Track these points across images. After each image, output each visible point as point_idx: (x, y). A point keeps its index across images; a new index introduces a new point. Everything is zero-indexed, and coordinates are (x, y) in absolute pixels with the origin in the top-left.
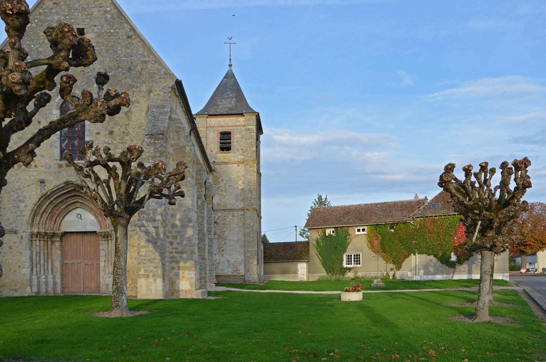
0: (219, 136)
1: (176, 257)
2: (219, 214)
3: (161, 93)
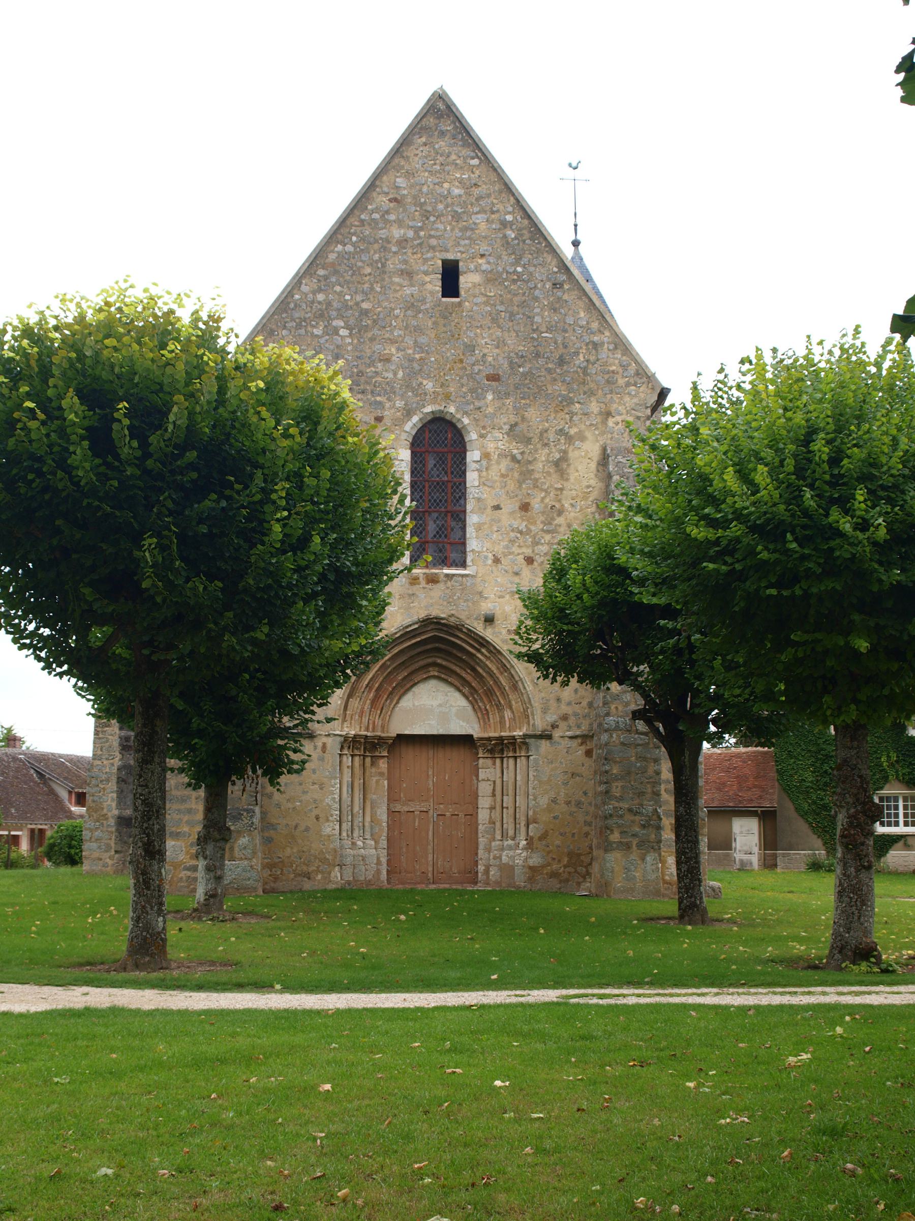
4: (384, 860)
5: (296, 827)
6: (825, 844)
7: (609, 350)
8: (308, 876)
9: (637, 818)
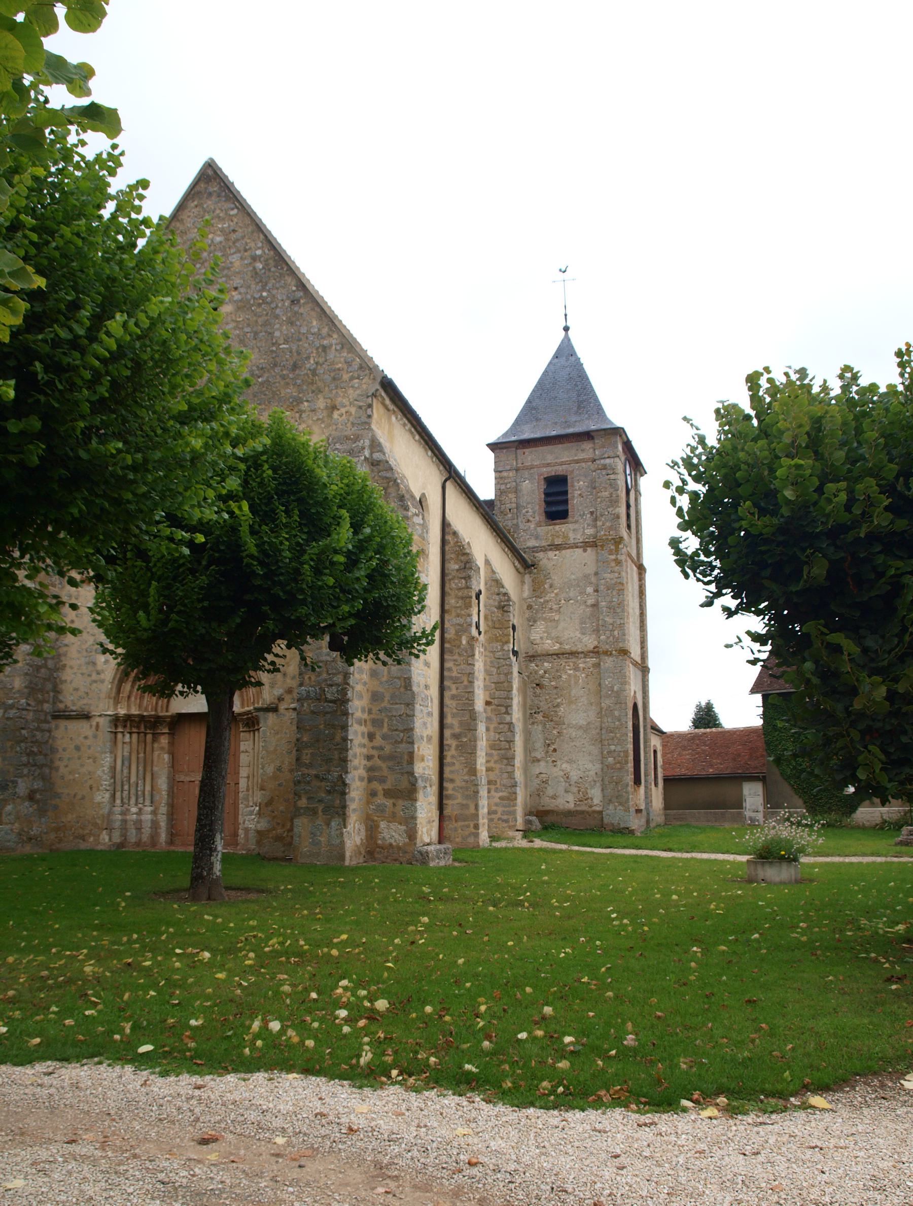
0: (543, 486)
1: (380, 769)
2: (546, 664)
3: (353, 410)
4: (163, 824)
5: (75, 796)
6: (805, 802)
7: (336, 350)
8: (83, 838)
9: (323, 784)
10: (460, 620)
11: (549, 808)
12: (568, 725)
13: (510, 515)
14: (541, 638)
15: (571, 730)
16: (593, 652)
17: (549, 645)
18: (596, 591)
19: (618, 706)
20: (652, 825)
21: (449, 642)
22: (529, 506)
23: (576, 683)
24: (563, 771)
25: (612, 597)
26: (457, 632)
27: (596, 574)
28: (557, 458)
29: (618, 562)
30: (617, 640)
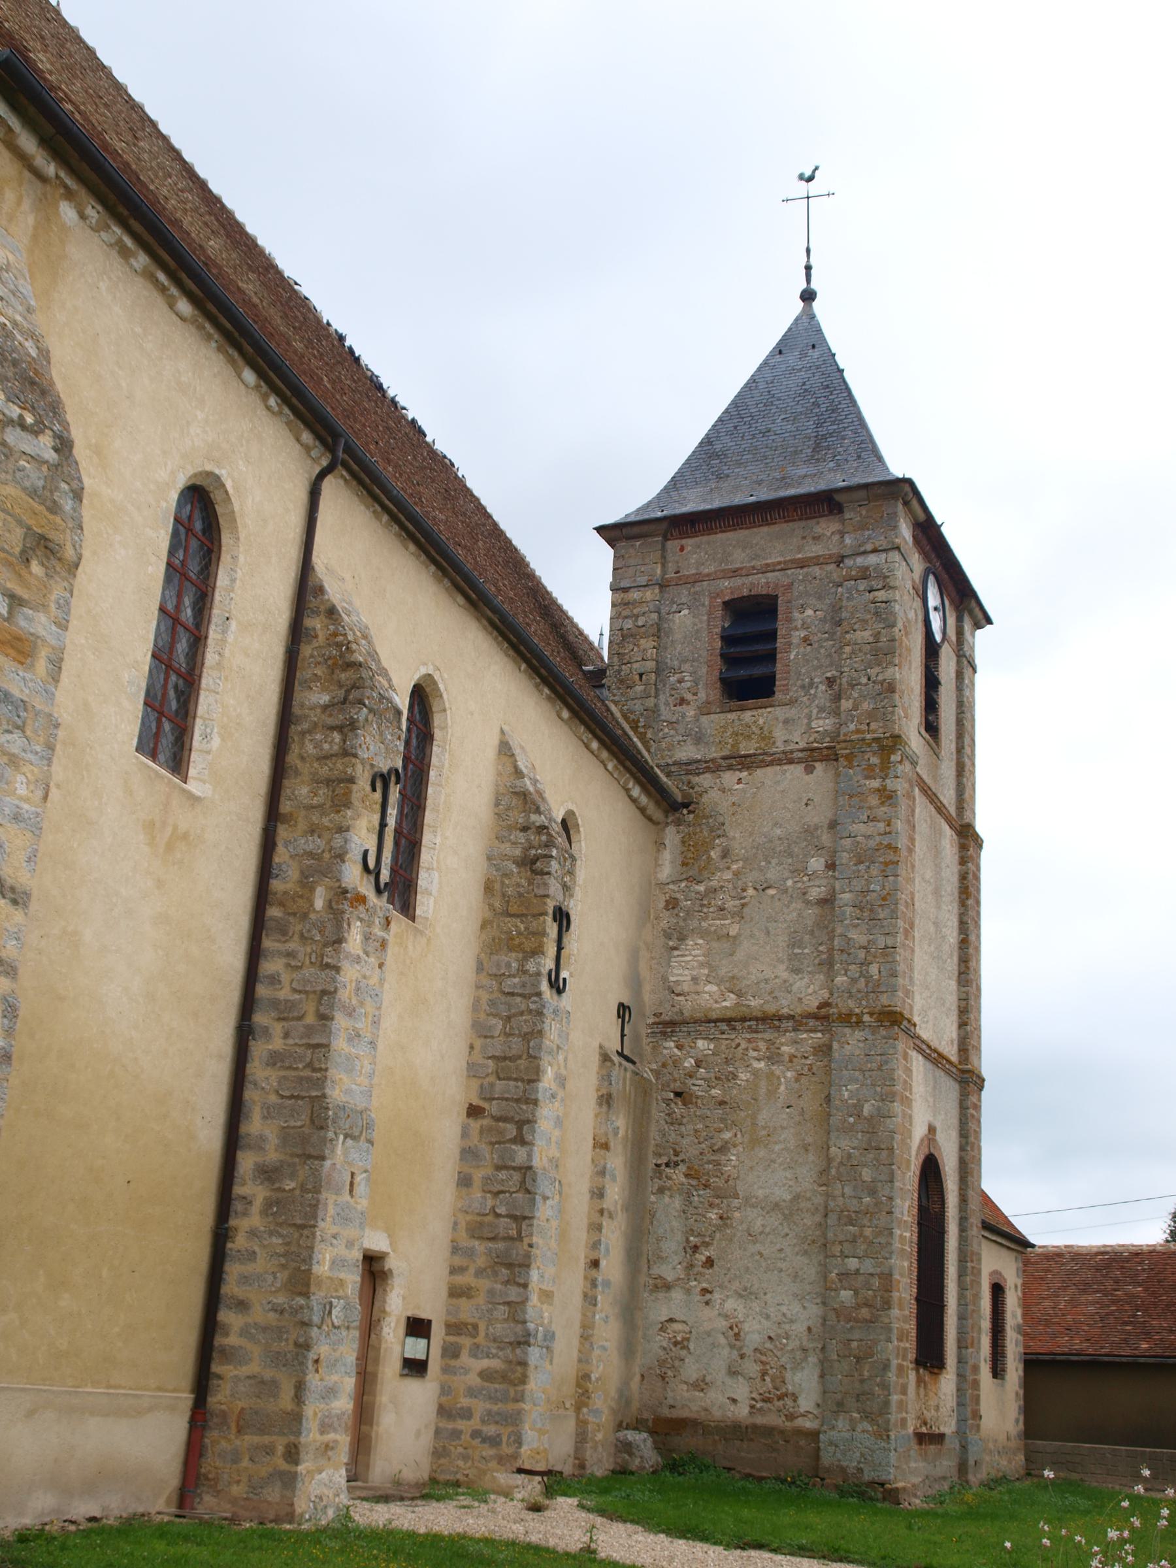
0: (720, 622)
2: (701, 1044)
10: (315, 843)
11: (685, 1414)
12: (747, 1199)
13: (639, 688)
14: (695, 979)
15: (751, 1213)
16: (815, 1017)
17: (712, 998)
18: (831, 866)
19: (871, 1156)
20: (975, 1478)
21: (281, 904)
22: (686, 667)
23: (772, 1093)
24: (726, 1317)
25: (868, 882)
26: (304, 875)
27: (833, 825)
28: (757, 557)
29: (887, 797)
30: (876, 989)
